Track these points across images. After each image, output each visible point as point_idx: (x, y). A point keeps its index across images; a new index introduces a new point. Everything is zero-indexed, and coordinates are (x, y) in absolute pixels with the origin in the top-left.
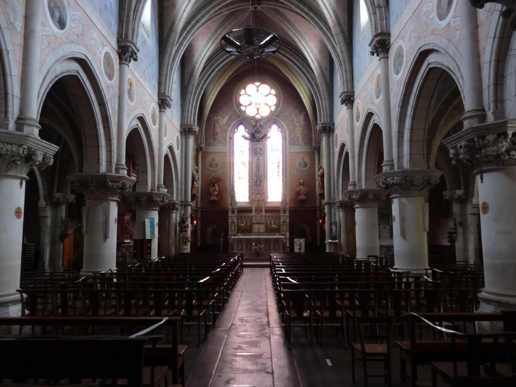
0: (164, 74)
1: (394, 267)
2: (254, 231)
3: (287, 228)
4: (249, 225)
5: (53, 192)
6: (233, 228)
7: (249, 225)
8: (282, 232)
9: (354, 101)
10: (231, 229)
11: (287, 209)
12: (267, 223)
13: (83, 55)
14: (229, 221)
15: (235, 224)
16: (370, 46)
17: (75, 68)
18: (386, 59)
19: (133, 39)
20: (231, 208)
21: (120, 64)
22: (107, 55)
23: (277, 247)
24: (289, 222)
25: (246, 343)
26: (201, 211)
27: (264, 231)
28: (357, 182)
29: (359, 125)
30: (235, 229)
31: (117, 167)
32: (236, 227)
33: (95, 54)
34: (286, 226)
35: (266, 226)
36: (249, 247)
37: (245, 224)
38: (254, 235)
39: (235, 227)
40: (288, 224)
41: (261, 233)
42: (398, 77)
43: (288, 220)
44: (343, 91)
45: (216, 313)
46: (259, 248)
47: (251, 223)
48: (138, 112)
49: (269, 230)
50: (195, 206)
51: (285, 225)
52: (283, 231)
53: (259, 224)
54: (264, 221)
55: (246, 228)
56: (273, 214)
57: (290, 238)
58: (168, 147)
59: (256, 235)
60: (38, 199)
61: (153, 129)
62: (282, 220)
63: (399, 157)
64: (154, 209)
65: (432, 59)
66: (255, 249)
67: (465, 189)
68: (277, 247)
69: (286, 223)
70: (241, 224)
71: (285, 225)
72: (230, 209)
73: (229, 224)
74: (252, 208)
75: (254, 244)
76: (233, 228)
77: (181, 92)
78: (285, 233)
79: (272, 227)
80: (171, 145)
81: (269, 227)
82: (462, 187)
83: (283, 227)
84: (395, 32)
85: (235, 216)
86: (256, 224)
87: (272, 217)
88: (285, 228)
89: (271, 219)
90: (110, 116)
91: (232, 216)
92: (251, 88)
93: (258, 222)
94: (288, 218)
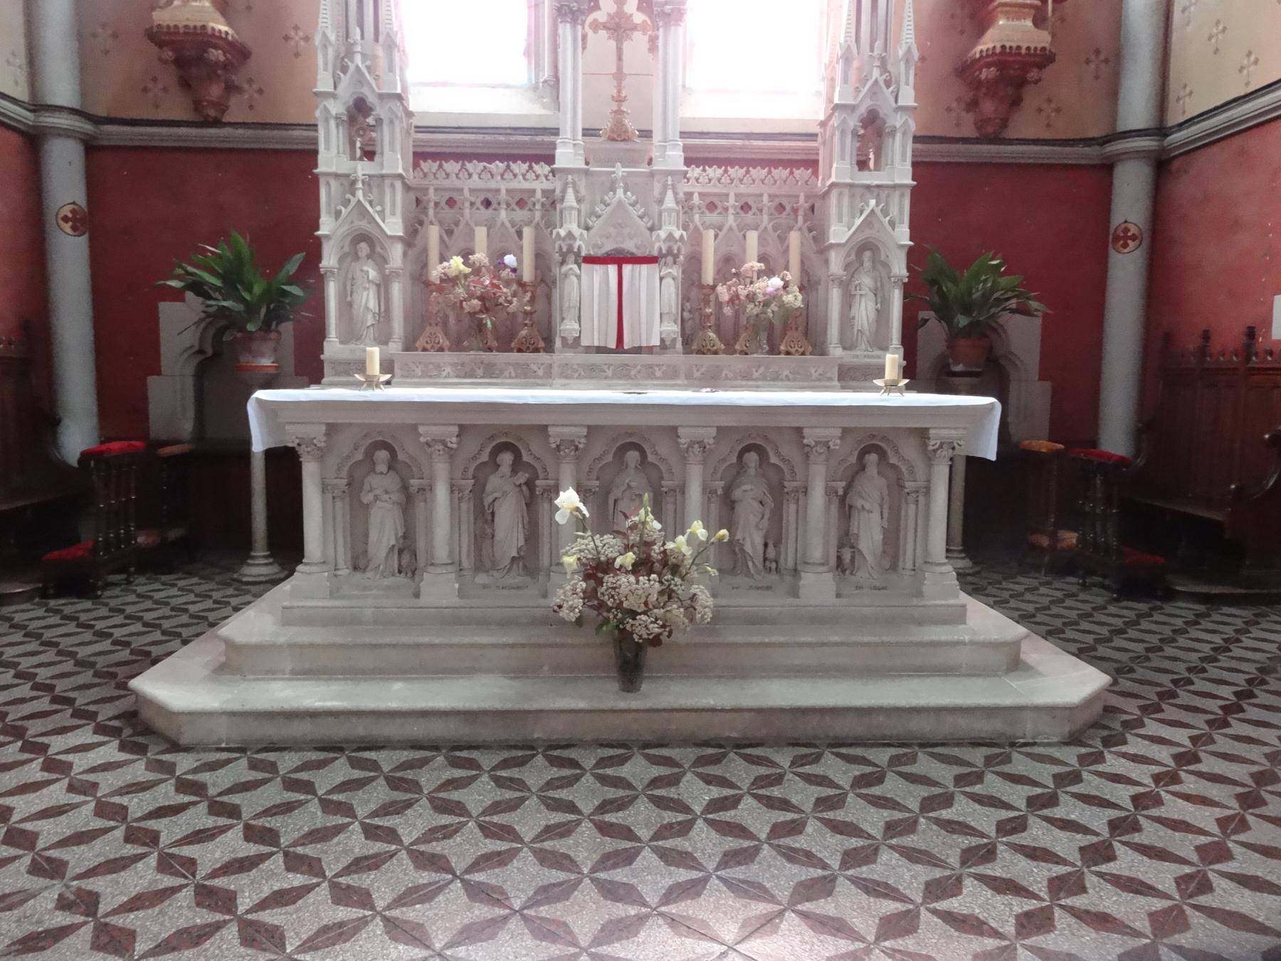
2: (568, 327)
3: (882, 315)
4: (528, 275)
6: (367, 299)
7: (528, 275)
8: (836, 351)
10: (346, 305)
11: (897, 121)
12: (695, 261)
14: (326, 226)
15: (381, 260)
20: (346, 93)
23: (870, 534)
24: (914, 256)
26: (91, 148)
27: (673, 328)
30: (385, 314)
32: (397, 290)
34: (880, 295)
35: (692, 282)
36: (508, 517)
37: (480, 256)
38: (569, 375)
39: (383, 288)
40: (900, 268)
41: (638, 350)
43: (903, 235)
45: (674, 158)
46: (643, 566)
47: (540, 257)
50: (22, 93)
51: (866, 281)
52: (847, 345)
53: (619, 259)
54: (671, 228)
55: (489, 303)
56: (756, 183)
59: (593, 374)
62: (839, 233)
66: (597, 570)
68: (870, 534)
69: (881, 264)
70: (443, 258)
71: (866, 281)
72: (336, 108)
73: (329, 260)
74: (555, 132)
75: (568, 499)
76: (367, 299)
78: (861, 356)
79: (751, 297)
81: (723, 292)
83: (848, 301)
85: (375, 182)
86: (590, 260)
87: (745, 207)
88: (864, 311)
89: (731, 220)
91: (349, 183)
93: (608, 247)
94: (901, 208)
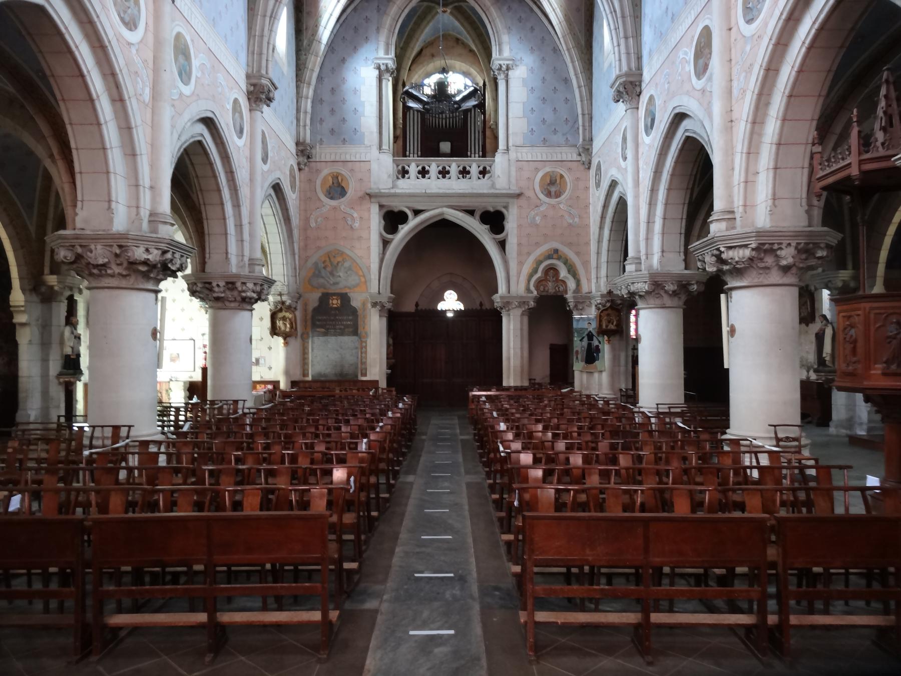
0: (257, 34)
1: (637, 405)
5: (42, 273)
9: (640, 93)
13: (211, 113)
16: (611, 87)
17: (201, 129)
18: (635, 110)
19: (267, 73)
21: (250, 110)
22: (236, 101)
25: (489, 75)
28: (643, 258)
29: (651, 142)
31: (152, 219)
33: (223, 106)
42: (597, 194)
44: (618, 72)
48: (202, 108)
49: (131, 505)
57: (12, 317)
58: (271, 185)
60: (8, 287)
61: (237, 145)
63: (647, 255)
64: (141, 286)
65: (686, 124)
67: (854, 268)
77: (297, 76)
80: (278, 181)
82: (850, 265)
84: (647, 76)
90: (88, 72)
92: (452, 292)
